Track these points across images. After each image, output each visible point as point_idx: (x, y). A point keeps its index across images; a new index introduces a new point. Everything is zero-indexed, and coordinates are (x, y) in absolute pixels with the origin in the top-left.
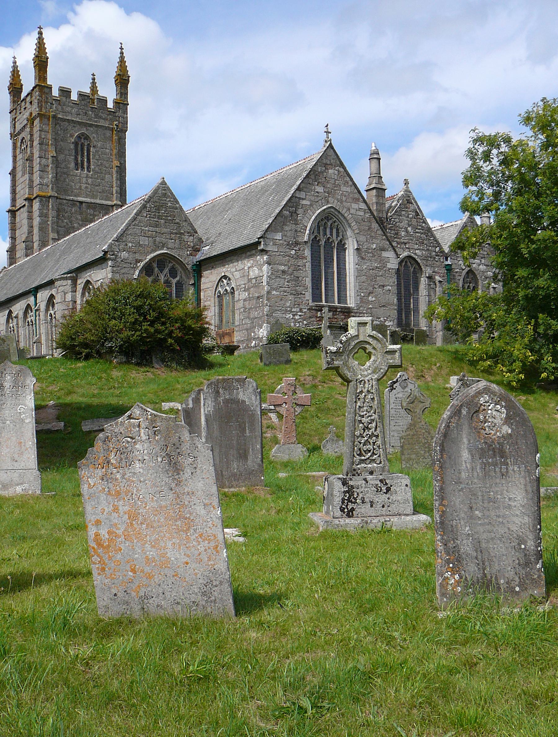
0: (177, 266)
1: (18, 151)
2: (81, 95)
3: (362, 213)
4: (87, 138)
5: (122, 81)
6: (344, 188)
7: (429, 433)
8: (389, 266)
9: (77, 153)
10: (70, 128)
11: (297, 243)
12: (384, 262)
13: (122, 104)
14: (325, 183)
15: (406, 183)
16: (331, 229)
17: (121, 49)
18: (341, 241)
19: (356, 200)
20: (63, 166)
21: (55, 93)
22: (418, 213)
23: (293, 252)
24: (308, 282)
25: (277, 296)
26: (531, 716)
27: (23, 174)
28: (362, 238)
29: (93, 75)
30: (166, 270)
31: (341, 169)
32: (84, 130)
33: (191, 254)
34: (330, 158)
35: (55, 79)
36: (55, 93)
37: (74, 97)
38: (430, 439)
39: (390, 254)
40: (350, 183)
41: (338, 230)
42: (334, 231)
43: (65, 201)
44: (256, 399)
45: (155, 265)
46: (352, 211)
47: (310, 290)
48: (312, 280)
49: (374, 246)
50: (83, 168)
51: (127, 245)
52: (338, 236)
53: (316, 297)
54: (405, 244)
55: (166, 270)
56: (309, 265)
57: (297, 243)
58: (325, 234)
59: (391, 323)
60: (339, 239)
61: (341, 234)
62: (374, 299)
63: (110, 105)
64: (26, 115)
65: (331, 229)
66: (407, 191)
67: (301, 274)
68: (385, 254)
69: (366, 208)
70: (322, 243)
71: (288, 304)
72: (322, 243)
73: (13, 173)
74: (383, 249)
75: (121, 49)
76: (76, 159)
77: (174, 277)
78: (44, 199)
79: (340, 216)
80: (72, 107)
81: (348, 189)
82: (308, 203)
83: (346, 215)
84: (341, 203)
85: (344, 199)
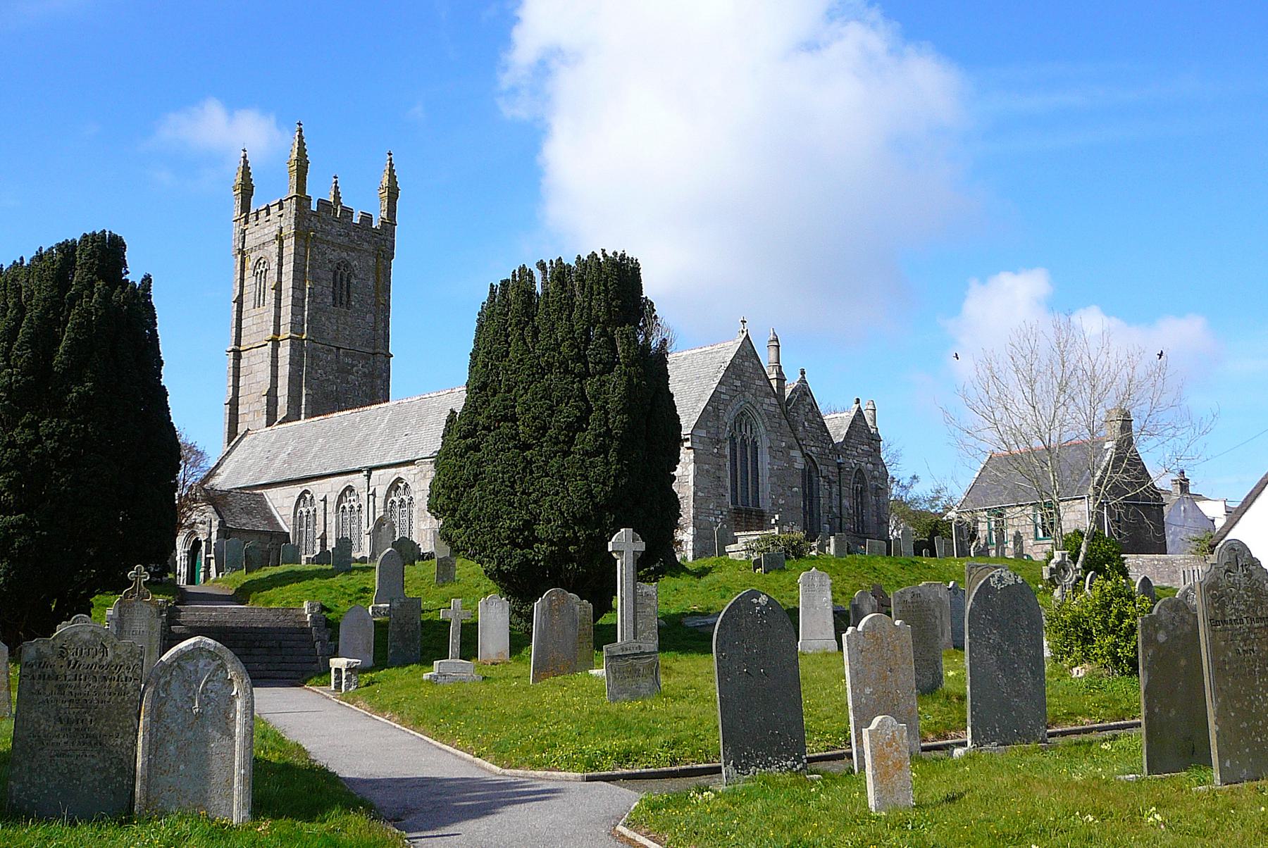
1: (248, 273)
2: (321, 202)
3: (772, 409)
4: (347, 265)
6: (757, 382)
9: (335, 285)
11: (719, 441)
12: (792, 460)
13: (390, 223)
15: (803, 373)
19: (768, 395)
22: (813, 405)
26: (1030, 780)
27: (257, 304)
28: (773, 436)
29: (744, 322)
34: (747, 352)
39: (796, 453)
44: (1018, 538)
46: (765, 406)
53: (734, 502)
56: (728, 464)
57: (719, 441)
64: (274, 230)
66: (803, 380)
73: (239, 301)
74: (791, 447)
76: (333, 292)
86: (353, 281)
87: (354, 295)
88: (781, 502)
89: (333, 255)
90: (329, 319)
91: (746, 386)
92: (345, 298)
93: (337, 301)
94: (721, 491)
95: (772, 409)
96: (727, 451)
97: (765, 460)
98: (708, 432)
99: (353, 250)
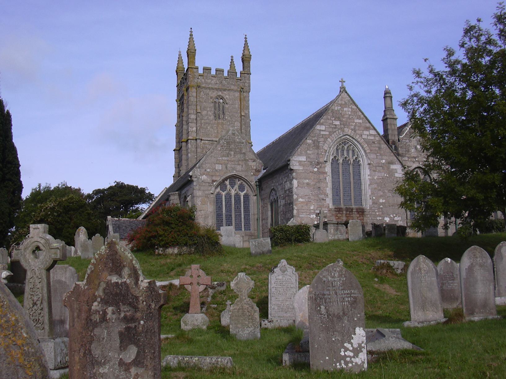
0: (244, 183)
3: (372, 138)
5: (246, 59)
7: (252, 308)
8: (397, 175)
9: (215, 109)
10: (210, 93)
12: (392, 173)
13: (246, 71)
14: (341, 118)
16: (348, 151)
17: (246, 38)
18: (356, 158)
20: (206, 118)
21: (201, 71)
23: (316, 170)
24: (329, 191)
25: (302, 202)
28: (372, 156)
29: (232, 57)
30: (236, 187)
31: (354, 107)
32: (220, 93)
33: (254, 175)
35: (200, 63)
36: (201, 71)
37: (213, 72)
38: (253, 312)
40: (362, 116)
41: (353, 151)
42: (351, 152)
43: (207, 142)
45: (227, 182)
46: (364, 137)
47: (330, 196)
48: (333, 188)
49: (384, 161)
50: (219, 118)
51: (206, 170)
52: (353, 155)
53: (335, 200)
54: (415, 158)
55: (236, 187)
56: (329, 179)
57: (318, 163)
58: (343, 154)
59: (400, 218)
60: (354, 157)
61: (356, 154)
62: (384, 201)
63: (238, 75)
65: (348, 151)
67: (322, 185)
68: (393, 167)
69: (376, 133)
70: (341, 161)
71: (312, 208)
72: (341, 161)
74: (392, 163)
75: (246, 38)
77: (242, 191)
78: (193, 141)
79: (354, 141)
80: (212, 80)
81: (361, 121)
82: (327, 133)
83: (359, 140)
84: (355, 131)
85: (357, 128)
86: (227, 106)
87: (227, 113)
88: (381, 201)
89: (214, 94)
90: (212, 127)
91: (345, 125)
92: (221, 116)
93: (217, 117)
94: (322, 196)
95: (372, 138)
96: (328, 168)
97: (366, 173)
98: (308, 157)
99: (225, 90)
